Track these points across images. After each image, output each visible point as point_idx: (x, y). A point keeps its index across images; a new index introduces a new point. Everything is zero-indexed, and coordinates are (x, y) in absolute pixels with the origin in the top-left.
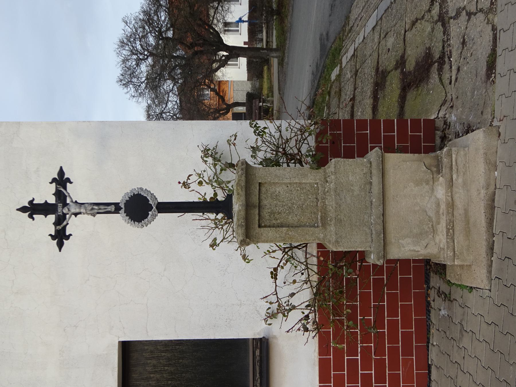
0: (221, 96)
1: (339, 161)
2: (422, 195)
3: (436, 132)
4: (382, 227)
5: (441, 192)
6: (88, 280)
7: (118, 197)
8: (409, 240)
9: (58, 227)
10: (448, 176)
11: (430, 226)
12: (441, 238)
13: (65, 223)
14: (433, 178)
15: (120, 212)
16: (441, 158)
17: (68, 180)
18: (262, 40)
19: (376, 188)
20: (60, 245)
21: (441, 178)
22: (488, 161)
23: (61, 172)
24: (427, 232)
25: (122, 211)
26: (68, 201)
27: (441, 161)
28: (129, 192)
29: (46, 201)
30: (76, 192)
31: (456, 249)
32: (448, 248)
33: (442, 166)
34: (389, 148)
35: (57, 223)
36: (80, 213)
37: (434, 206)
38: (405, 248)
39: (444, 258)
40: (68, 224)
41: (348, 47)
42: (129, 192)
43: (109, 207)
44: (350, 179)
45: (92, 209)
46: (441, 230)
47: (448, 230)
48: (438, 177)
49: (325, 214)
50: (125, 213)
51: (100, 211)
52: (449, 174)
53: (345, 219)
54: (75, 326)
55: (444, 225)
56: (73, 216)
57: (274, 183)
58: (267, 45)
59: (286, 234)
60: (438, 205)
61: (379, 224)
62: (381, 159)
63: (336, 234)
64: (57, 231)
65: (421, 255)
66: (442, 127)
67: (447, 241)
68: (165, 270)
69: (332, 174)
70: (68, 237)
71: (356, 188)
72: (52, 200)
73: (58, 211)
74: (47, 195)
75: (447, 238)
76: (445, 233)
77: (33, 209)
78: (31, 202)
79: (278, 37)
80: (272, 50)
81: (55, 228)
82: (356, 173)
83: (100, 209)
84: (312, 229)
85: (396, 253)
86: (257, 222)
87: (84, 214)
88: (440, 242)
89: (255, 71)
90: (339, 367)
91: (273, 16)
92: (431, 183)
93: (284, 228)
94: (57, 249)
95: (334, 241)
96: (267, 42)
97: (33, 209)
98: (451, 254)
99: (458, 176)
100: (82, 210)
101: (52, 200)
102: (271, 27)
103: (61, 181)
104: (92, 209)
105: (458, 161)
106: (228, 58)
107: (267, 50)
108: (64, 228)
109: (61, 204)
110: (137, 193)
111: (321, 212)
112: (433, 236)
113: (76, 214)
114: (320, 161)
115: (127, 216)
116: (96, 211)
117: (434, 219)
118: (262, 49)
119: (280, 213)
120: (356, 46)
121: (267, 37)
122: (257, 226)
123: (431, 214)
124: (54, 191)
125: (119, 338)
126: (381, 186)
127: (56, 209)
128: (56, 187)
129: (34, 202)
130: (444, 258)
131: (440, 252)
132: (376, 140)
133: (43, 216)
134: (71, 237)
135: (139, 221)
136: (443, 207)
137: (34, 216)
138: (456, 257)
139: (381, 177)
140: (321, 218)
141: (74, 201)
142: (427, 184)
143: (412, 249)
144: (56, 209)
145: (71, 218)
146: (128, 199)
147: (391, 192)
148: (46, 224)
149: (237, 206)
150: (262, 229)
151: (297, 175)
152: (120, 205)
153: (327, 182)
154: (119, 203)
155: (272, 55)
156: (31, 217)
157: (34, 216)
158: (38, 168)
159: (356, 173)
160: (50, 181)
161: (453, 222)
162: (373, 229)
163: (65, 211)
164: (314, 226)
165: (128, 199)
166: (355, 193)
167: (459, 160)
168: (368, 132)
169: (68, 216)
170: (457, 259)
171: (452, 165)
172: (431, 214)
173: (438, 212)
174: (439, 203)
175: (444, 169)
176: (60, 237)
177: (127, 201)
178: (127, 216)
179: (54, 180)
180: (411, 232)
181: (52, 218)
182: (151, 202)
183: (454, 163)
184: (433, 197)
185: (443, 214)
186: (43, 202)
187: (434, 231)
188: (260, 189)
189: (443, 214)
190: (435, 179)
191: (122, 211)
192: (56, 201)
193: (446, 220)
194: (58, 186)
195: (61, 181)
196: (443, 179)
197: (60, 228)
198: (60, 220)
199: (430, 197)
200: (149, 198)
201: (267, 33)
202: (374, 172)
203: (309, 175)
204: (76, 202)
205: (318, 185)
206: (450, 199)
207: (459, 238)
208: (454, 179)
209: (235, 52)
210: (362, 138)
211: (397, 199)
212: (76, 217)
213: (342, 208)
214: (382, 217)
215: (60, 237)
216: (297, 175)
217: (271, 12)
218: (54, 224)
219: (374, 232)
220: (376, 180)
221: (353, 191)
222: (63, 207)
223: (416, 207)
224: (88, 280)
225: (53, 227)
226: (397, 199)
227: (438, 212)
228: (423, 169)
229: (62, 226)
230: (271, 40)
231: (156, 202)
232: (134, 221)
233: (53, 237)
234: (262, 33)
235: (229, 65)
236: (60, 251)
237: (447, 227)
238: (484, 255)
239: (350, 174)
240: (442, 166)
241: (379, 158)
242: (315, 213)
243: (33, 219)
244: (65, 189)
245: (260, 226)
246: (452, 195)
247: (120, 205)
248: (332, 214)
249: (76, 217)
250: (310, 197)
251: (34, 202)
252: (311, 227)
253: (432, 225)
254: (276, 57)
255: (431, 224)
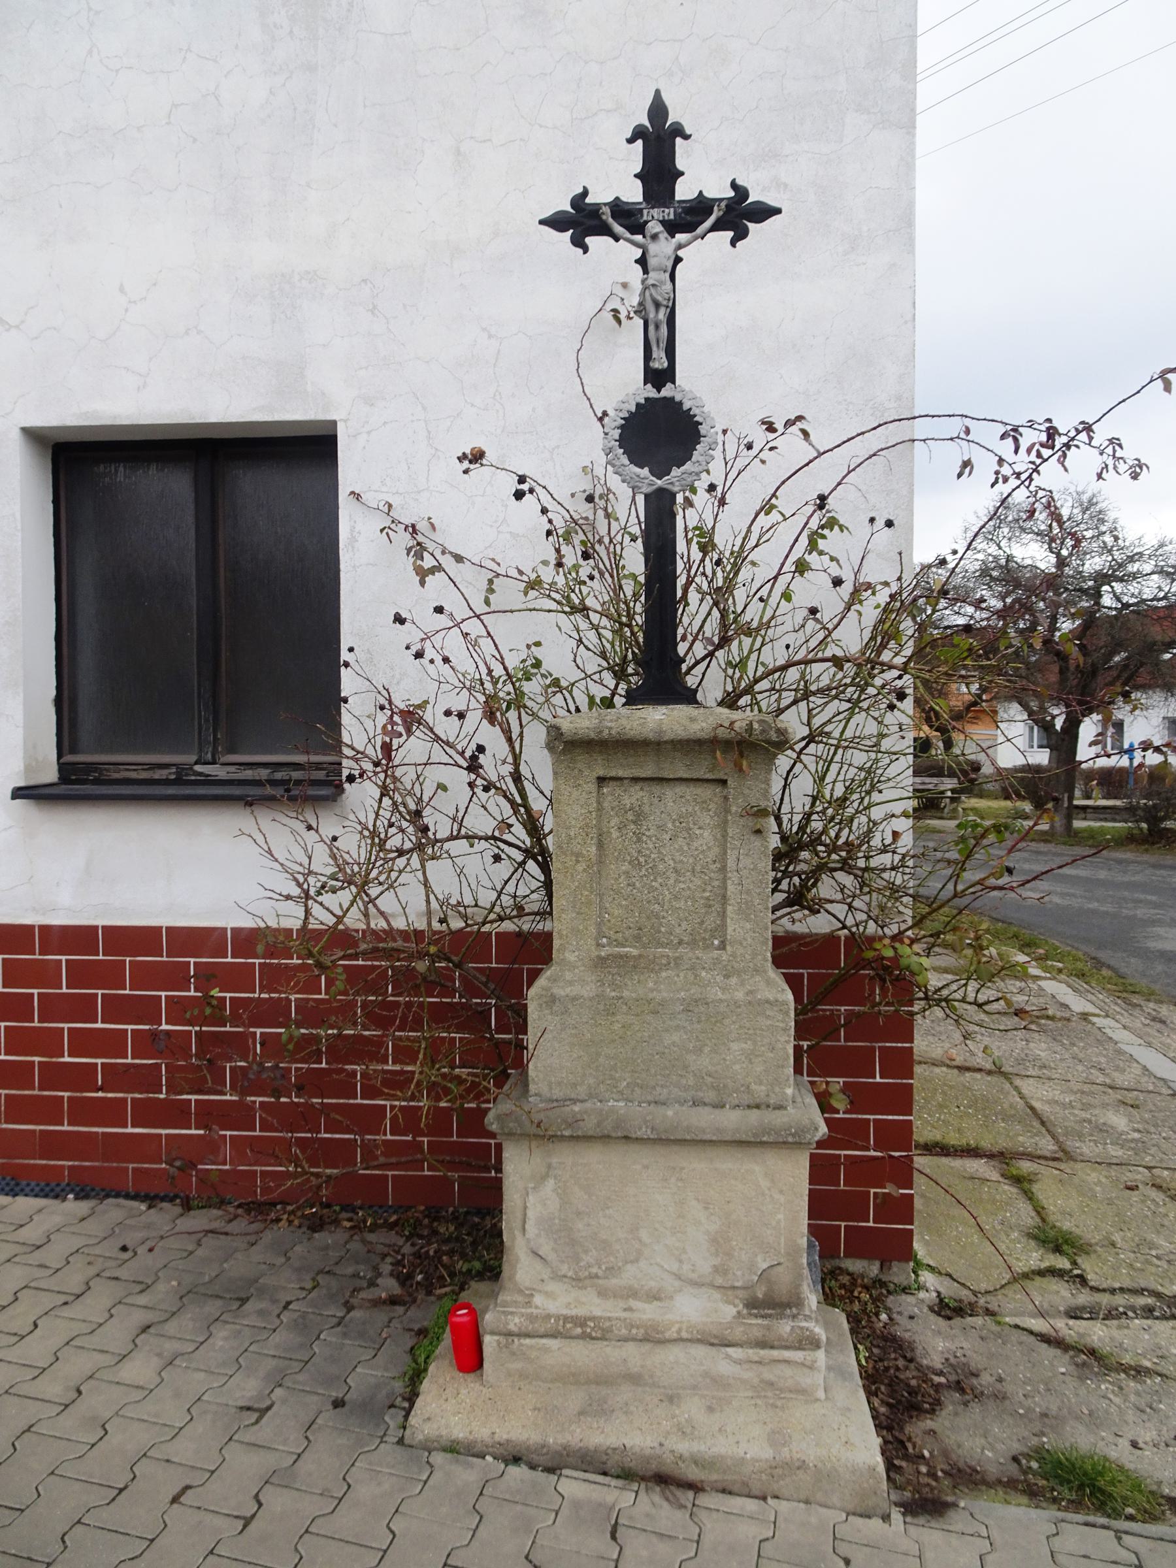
0: (972, 711)
1: (787, 1013)
2: (684, 1251)
3: (878, 1263)
4: (590, 1133)
5: (692, 1309)
6: (490, 336)
7: (692, 383)
8: (554, 1204)
9: (607, 210)
10: (738, 1333)
11: (594, 1270)
12: (557, 1300)
13: (618, 229)
14: (734, 1288)
15: (649, 385)
16: (794, 1317)
17: (740, 235)
18: (1089, 797)
19: (704, 1120)
20: (556, 222)
21: (734, 1311)
22: (779, 1471)
23: (764, 212)
24: (577, 1259)
25: (651, 392)
26: (681, 237)
27: (782, 1316)
28: (706, 409)
29: (682, 174)
30: (707, 251)
31: (528, 1341)
32: (532, 1318)
33: (770, 1316)
34: (821, 1170)
35: (621, 211)
36: (646, 271)
37: (652, 1284)
38: (535, 1194)
39: (505, 1304)
40: (617, 239)
41: (1090, 997)
42: (706, 409)
43: (663, 355)
44: (735, 1046)
45: (657, 305)
46: (584, 1300)
47: (581, 1322)
48: (737, 1301)
49: (635, 967)
50: (646, 399)
51: (651, 328)
52: (744, 1338)
53: (617, 1026)
54: (375, 307)
55: (598, 1312)
56: (638, 253)
57: (726, 822)
58: (1077, 807)
59: (578, 855)
60: (655, 1296)
61: (599, 1124)
62: (790, 1139)
63: (574, 999)
64: (595, 211)
65: (514, 1238)
66: (891, 1279)
67: (549, 1316)
68: (514, 536)
69: (750, 992)
70: (579, 242)
71: (704, 1062)
72: (684, 191)
73: (653, 208)
74: (700, 175)
75: (558, 1318)
76: (574, 1312)
77: (659, 141)
78: (678, 131)
79: (1090, 830)
80: (1069, 818)
81: (605, 204)
82: (751, 1062)
83: (657, 327)
84: (593, 930)
85: (519, 1168)
86: (613, 774)
87: (643, 282)
88: (547, 1294)
89: (1027, 784)
90: (146, 976)
91: (1147, 821)
92: (719, 1281)
93: (594, 849)
94: (547, 213)
95: (555, 991)
96: (1084, 808)
97: (659, 141)
98: (512, 1327)
99: (738, 1362)
100: (653, 277)
101: (684, 191)
102: (1117, 817)
103: (740, 214)
104: (657, 305)
105: (782, 1366)
106: (1047, 727)
107: (1068, 808)
108: (604, 230)
109: (672, 217)
110: (703, 432)
111: (640, 956)
112: (565, 1276)
113: (642, 262)
114: (789, 953)
115: (638, 405)
116: (652, 315)
117: (614, 1281)
118: (1071, 798)
119: (639, 840)
120: (1094, 1019)
121: (1096, 809)
122: (601, 773)
123: (630, 1276)
124: (709, 194)
125: (345, 421)
126: (708, 1137)
127: (661, 202)
128: (721, 200)
129: (678, 140)
130: (505, 1304)
131: (520, 1291)
132: (860, 1098)
133: (638, 168)
134: (580, 251)
135: (622, 441)
136: (647, 1312)
137: (639, 143)
138: (502, 1339)
139: (737, 1137)
140: (621, 957)
141: (680, 253)
142: (716, 1269)
143: (530, 1213)
144: (661, 202)
145: (634, 248)
146: (685, 407)
147: (695, 1164)
148: (618, 179)
149: (658, 718)
150: (593, 787)
151: (748, 892)
152: (669, 385)
153: (727, 977)
154: (674, 382)
155: (1057, 819)
156: (638, 134)
157: (639, 143)
158: (786, 185)
159: (751, 1062)
160: (739, 182)
161: (603, 1338)
162: (588, 1105)
163: (654, 227)
164: (600, 934)
165: (685, 407)
166: (691, 1058)
167: (788, 1371)
168: (878, 1079)
169: (639, 238)
170: (499, 1343)
171: (772, 1347)
172: (630, 1276)
173: (633, 1293)
174: (659, 1299)
175: (760, 1321)
176: (582, 221)
177: (681, 403)
178: (638, 405)
179: (741, 192)
180: (578, 1214)
181: (633, 193)
182: (676, 472)
183: (775, 1353)
184: (677, 1283)
185: (629, 1309)
186: (680, 164)
187: (577, 1281)
188: (707, 781)
189: (629, 1309)
190: (730, 1293)
191: (651, 392)
192: (679, 202)
193: (609, 1319)
194: (723, 204)
195: (740, 214)
196: (729, 1319)
197: (604, 217)
198: (628, 218)
199: (678, 1277)
200: (688, 466)
201: (1105, 808)
202: (754, 1116)
203: (748, 926)
204: (678, 260)
205: (718, 948)
206: (672, 1334)
207: (558, 1353)
208: (730, 1350)
209: (1063, 743)
210: (858, 1063)
211: (673, 1180)
212: (637, 261)
213: (649, 1018)
214: (619, 1134)
215: (582, 221)
216: (748, 892)
217: (1152, 816)
218: (617, 198)
219: (576, 1108)
220: (731, 1120)
221: (699, 1051)
222: (663, 222)
223: (649, 1237)
224: (490, 336)
225: (610, 199)
226: (673, 1180)
227: (633, 1293)
228: (759, 1259)
229: (610, 220)
230: (1089, 816)
231: (676, 489)
232: (622, 427)
233: (579, 201)
234: (1104, 798)
235: (1032, 729)
236: (541, 222)
237: (593, 1319)
238: (502, 1435)
239: (748, 1045)
240: (770, 1316)
241: (793, 1135)
242: (638, 938)
243: (630, 141)
244: (715, 228)
245: (601, 780)
246: (682, 1340)
247: (669, 385)
248: (633, 989)
249: (637, 261)
250: (684, 925)
251: (678, 140)
252: (599, 925)
253: (597, 1276)
254: (1052, 827)
255: (600, 1273)
